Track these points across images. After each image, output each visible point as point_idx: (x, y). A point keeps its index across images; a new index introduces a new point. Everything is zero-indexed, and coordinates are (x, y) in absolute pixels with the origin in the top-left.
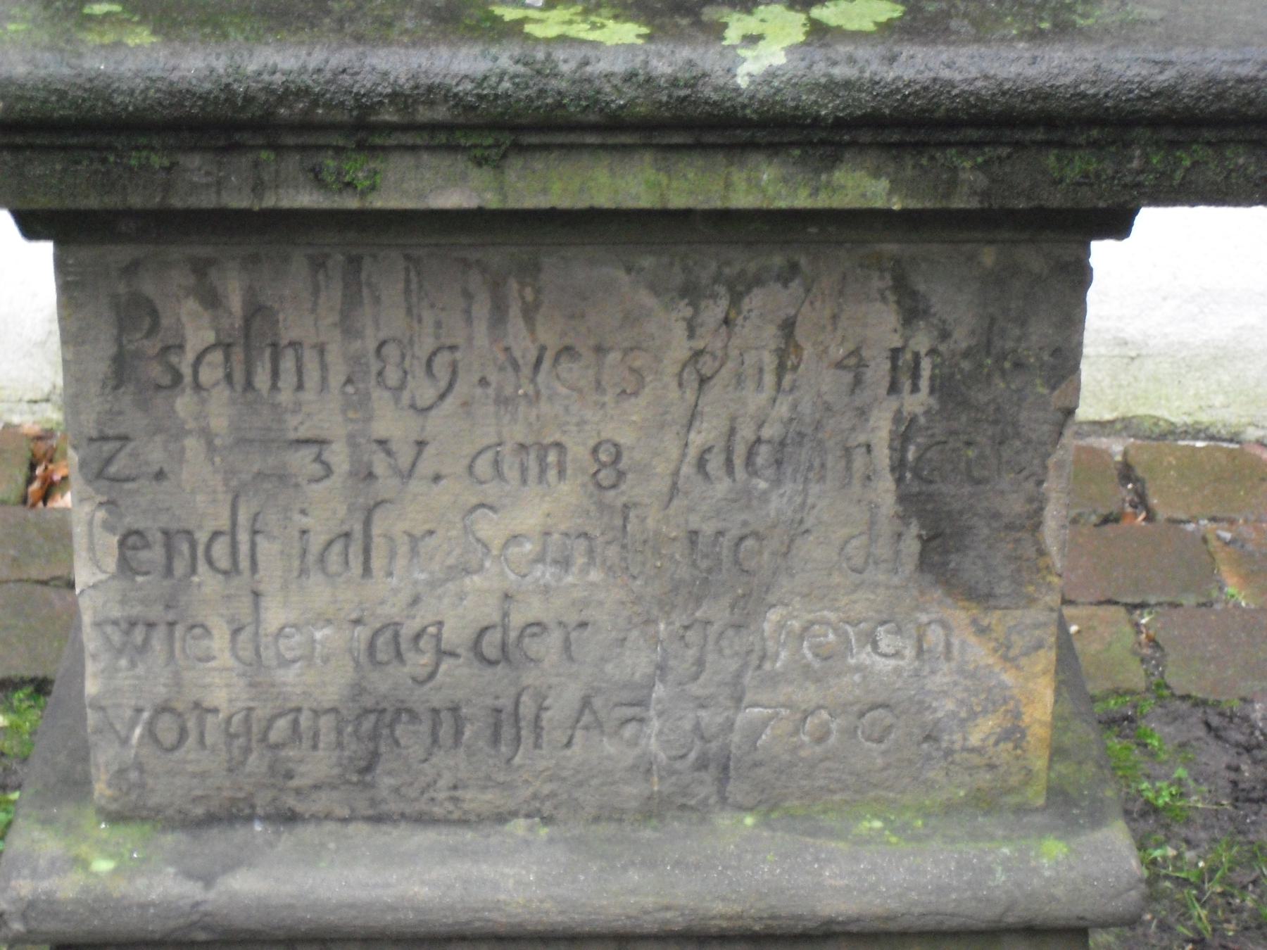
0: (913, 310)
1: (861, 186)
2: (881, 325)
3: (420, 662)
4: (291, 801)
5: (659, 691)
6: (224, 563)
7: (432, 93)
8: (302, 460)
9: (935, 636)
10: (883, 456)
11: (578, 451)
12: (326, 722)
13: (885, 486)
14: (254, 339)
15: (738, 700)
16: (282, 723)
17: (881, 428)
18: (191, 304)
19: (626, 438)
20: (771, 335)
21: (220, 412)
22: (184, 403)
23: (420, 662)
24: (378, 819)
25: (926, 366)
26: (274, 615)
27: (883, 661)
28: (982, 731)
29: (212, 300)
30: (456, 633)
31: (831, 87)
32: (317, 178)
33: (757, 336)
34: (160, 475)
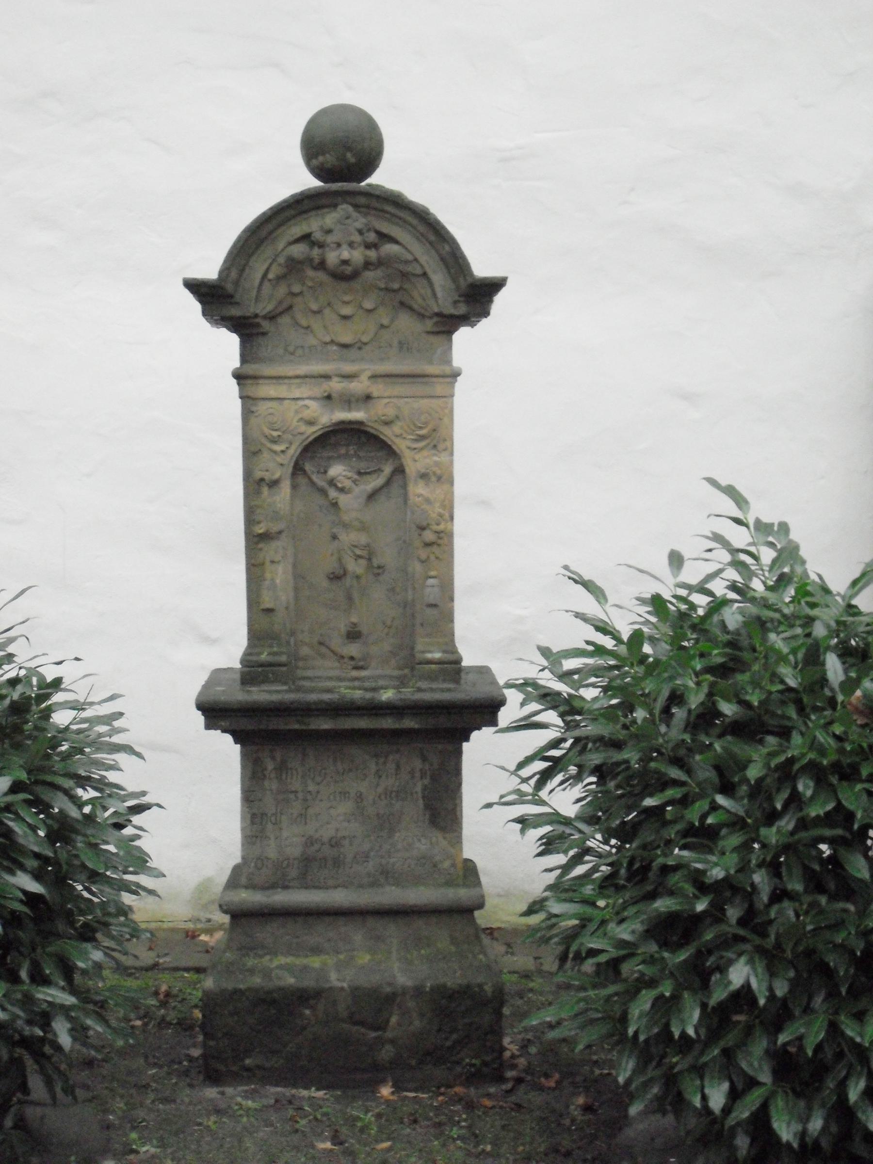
0: (424, 759)
1: (409, 723)
2: (418, 764)
3: (316, 847)
4: (287, 883)
5: (372, 854)
6: (274, 821)
7: (321, 702)
8: (292, 796)
9: (434, 839)
10: (420, 795)
11: (352, 795)
12: (296, 862)
13: (421, 802)
14: (282, 768)
15: (389, 856)
16: (286, 862)
17: (419, 788)
18: (269, 759)
19: (363, 790)
20: (393, 766)
21: (275, 786)
22: (266, 783)
23: (316, 847)
24: (306, 888)
25: (428, 773)
26: (285, 834)
27: (422, 846)
28: (447, 864)
29: (273, 758)
30: (325, 839)
31: (401, 699)
32: (298, 722)
33: (391, 766)
34: (260, 800)
